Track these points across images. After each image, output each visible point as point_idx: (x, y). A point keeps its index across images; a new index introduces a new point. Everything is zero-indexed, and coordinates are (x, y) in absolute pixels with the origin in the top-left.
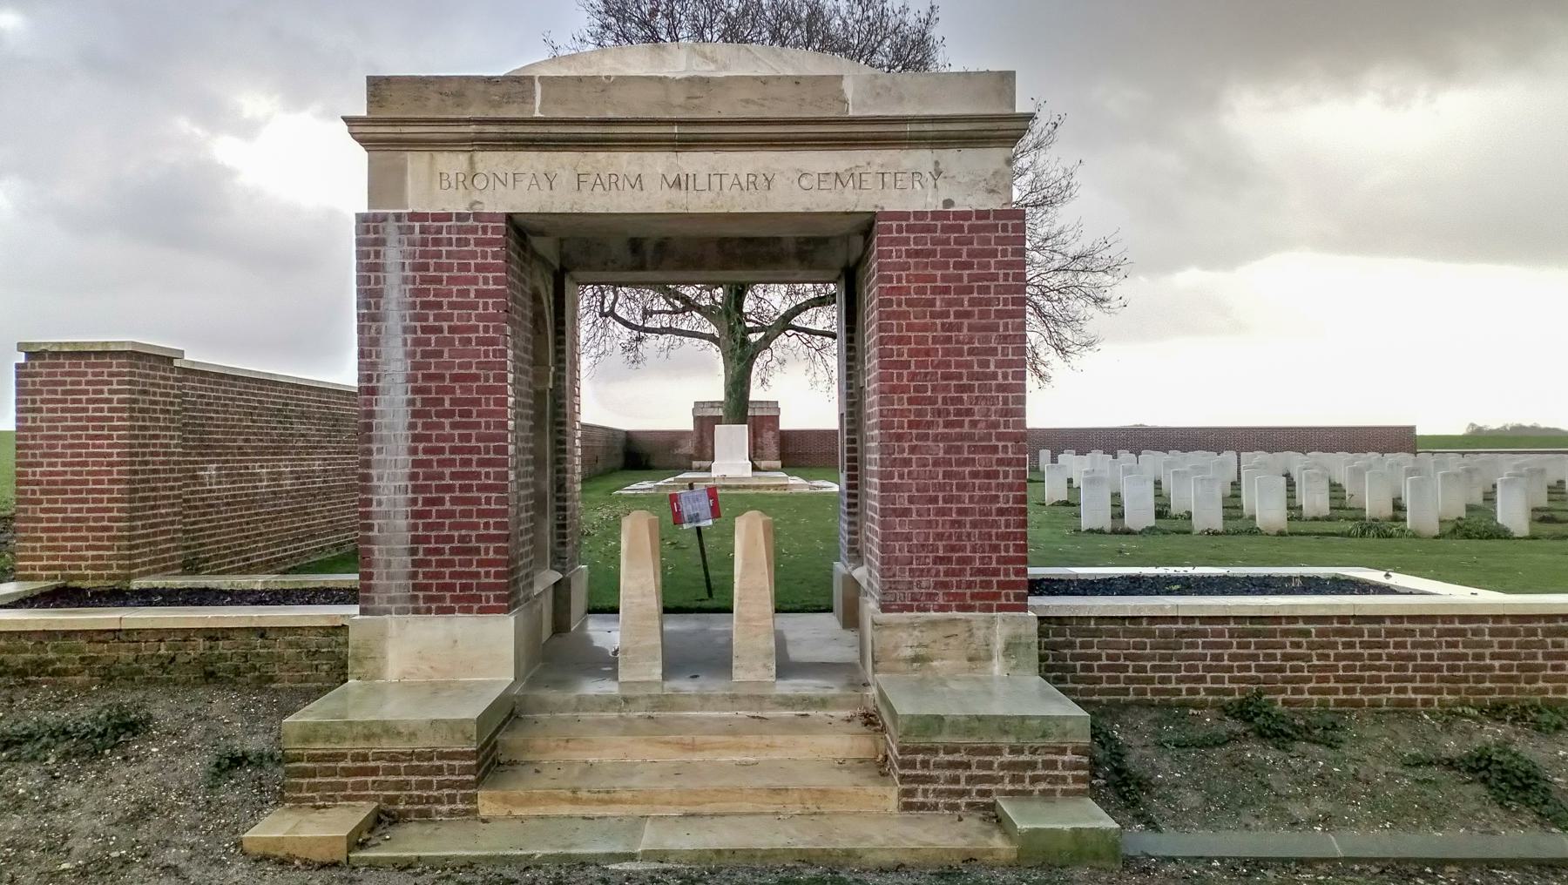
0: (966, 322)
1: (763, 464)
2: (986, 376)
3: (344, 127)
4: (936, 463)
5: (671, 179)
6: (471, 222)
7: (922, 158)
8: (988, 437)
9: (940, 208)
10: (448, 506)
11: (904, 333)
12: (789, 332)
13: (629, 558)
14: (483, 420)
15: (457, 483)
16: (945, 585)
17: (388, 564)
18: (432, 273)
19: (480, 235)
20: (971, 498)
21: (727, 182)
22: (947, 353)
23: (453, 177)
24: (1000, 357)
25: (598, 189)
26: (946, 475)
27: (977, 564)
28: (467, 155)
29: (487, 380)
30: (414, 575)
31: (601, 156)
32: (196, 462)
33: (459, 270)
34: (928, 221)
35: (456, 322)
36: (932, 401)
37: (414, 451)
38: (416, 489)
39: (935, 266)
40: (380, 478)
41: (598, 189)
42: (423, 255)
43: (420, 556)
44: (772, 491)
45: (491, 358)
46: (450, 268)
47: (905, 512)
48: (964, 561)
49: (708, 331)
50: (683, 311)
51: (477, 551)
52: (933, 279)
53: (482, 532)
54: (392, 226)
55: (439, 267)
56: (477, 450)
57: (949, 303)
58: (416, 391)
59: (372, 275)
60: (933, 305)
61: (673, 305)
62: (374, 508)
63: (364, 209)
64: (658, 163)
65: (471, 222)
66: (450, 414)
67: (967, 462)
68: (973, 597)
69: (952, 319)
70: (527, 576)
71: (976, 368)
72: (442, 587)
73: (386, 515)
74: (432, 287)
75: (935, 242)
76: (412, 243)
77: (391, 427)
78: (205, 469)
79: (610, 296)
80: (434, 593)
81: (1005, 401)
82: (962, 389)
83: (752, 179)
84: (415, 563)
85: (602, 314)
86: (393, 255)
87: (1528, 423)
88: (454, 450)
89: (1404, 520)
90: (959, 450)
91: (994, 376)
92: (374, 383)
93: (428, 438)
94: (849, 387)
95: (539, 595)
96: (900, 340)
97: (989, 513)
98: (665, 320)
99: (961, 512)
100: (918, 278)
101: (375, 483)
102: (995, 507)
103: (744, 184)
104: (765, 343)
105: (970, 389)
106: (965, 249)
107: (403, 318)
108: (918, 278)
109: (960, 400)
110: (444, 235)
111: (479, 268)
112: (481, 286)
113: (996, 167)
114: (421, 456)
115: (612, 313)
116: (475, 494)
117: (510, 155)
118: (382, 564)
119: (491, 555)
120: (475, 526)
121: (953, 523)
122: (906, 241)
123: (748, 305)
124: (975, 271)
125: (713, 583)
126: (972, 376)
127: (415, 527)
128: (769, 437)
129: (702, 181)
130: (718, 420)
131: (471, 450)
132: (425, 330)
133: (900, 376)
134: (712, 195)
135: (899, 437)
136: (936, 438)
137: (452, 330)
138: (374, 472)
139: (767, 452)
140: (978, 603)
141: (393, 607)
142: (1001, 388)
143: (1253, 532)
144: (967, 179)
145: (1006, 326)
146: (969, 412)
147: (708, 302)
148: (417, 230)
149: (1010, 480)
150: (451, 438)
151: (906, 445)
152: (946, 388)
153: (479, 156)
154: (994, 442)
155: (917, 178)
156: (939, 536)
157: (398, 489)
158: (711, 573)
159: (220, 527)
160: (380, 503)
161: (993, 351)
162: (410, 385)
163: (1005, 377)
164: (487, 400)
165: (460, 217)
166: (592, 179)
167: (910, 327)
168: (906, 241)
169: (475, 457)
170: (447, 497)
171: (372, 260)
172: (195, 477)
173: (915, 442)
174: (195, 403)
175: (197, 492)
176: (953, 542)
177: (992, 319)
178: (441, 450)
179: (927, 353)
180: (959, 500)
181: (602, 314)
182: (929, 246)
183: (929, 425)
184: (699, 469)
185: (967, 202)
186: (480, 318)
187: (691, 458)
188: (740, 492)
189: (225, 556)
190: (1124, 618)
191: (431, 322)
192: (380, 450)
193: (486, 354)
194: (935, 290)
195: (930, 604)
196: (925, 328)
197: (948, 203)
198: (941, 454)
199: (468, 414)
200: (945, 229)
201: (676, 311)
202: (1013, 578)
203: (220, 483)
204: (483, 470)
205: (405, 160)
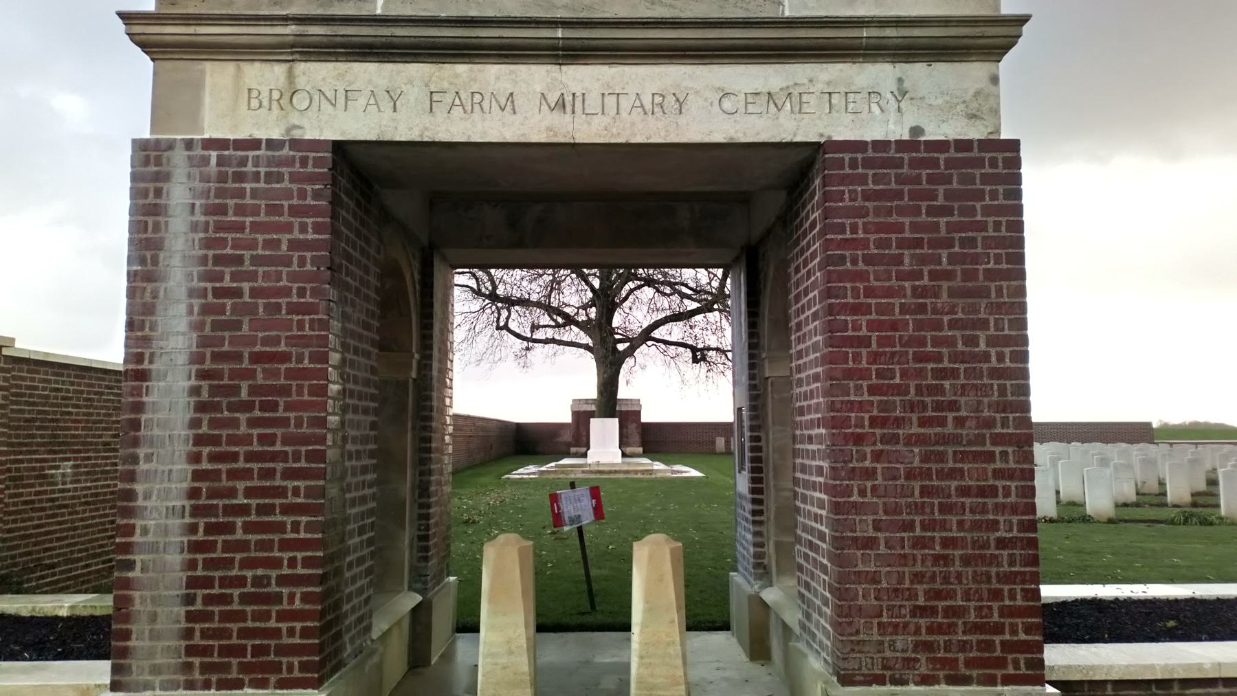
0: (945, 285)
1: (628, 450)
2: (975, 357)
3: (120, 25)
4: (910, 475)
5: (553, 98)
6: (286, 151)
7: (882, 74)
8: (980, 439)
9: (906, 137)
10: (239, 535)
11: (862, 300)
12: (649, 343)
13: (491, 601)
14: (292, 415)
15: (254, 502)
16: (928, 647)
17: (153, 618)
18: (231, 218)
19: (297, 168)
20: (960, 524)
21: (626, 103)
22: (919, 325)
23: (265, 94)
24: (992, 331)
25: (457, 111)
26: (925, 491)
27: (972, 617)
28: (284, 67)
29: (300, 360)
30: (188, 634)
31: (462, 69)
32: (45, 460)
33: (268, 213)
34: (892, 153)
35: (260, 283)
36: (901, 390)
37: (195, 458)
38: (197, 511)
39: (902, 211)
40: (147, 496)
41: (457, 111)
42: (220, 193)
43: (199, 606)
44: (639, 476)
45: (307, 332)
46: (255, 211)
47: (870, 543)
48: (952, 612)
49: (584, 342)
50: (564, 325)
51: (278, 598)
52: (899, 228)
53: (286, 571)
54: (179, 157)
55: (241, 210)
56: (283, 456)
57: (923, 260)
58: (202, 375)
59: (150, 220)
60: (901, 263)
61: (555, 321)
62: (137, 538)
63: (146, 135)
64: (535, 78)
65: (286, 151)
66: (247, 406)
67: (952, 474)
68: (969, 663)
69: (926, 281)
70: (360, 620)
71: (960, 347)
72: (228, 651)
73: (153, 548)
74: (230, 236)
75: (901, 180)
76: (205, 179)
77: (163, 424)
78: (57, 468)
79: (504, 313)
80: (216, 659)
81: (1002, 390)
82: (941, 374)
83: (658, 99)
84: (191, 617)
85: (498, 328)
86: (179, 194)
87: (1201, 419)
88: (252, 457)
89: (1218, 506)
90: (941, 457)
91: (986, 357)
92: (146, 365)
93: (215, 441)
94: (752, 377)
95: (385, 635)
96: (856, 309)
97: (985, 545)
98: (550, 333)
99: (947, 543)
100: (881, 228)
101: (140, 502)
102: (993, 536)
103: (648, 107)
104: (630, 352)
105: (954, 373)
106: (941, 189)
107: (189, 276)
108: (881, 228)
109: (939, 390)
110: (250, 168)
111: (294, 211)
112: (296, 235)
113: (978, 86)
114: (205, 465)
115: (506, 327)
116: (279, 518)
117: (342, 66)
118: (144, 617)
119: (297, 604)
120: (277, 563)
121: (936, 558)
122: (863, 180)
123: (617, 321)
124: (956, 218)
125: (595, 586)
126: (955, 357)
127: (192, 565)
128: (632, 427)
129: (593, 103)
130: (592, 414)
131: (274, 457)
132: (218, 293)
133: (857, 357)
134: (606, 120)
135: (859, 439)
136: (910, 441)
137: (255, 293)
138: (139, 488)
139: (631, 440)
140: (975, 673)
141: (158, 680)
142: (996, 373)
143: (1086, 519)
144: (940, 101)
145: (999, 291)
146: (953, 406)
147: (584, 318)
148: (213, 161)
149: (1013, 499)
150: (247, 440)
151: (868, 450)
152: (920, 373)
153: (301, 67)
154: (989, 447)
155: (874, 98)
156: (918, 577)
157: (171, 511)
158: (594, 572)
159: (75, 529)
160: (145, 531)
161: (984, 324)
162: (194, 368)
163: (1000, 358)
164: (300, 387)
165: (271, 144)
166: (448, 98)
167: (870, 292)
168: (863, 180)
169: (280, 466)
170: (239, 521)
171: (151, 199)
172: (45, 476)
173: (879, 447)
174: (47, 397)
175: (45, 492)
176: (937, 586)
177: (981, 281)
178: (234, 457)
179: (894, 326)
180: (943, 526)
181: (498, 328)
182: (893, 186)
183: (899, 422)
184: (576, 455)
185: (942, 129)
186: (293, 277)
187: (569, 445)
188: (612, 476)
189: (80, 559)
190: (1149, 682)
191: (227, 283)
192: (149, 458)
193: (301, 326)
194: (902, 244)
195: (909, 674)
196: (890, 292)
197: (917, 130)
198: (916, 463)
199: (274, 407)
200: (914, 164)
201: (558, 326)
202: (1023, 636)
203: (78, 481)
204: (291, 484)
205: (203, 72)
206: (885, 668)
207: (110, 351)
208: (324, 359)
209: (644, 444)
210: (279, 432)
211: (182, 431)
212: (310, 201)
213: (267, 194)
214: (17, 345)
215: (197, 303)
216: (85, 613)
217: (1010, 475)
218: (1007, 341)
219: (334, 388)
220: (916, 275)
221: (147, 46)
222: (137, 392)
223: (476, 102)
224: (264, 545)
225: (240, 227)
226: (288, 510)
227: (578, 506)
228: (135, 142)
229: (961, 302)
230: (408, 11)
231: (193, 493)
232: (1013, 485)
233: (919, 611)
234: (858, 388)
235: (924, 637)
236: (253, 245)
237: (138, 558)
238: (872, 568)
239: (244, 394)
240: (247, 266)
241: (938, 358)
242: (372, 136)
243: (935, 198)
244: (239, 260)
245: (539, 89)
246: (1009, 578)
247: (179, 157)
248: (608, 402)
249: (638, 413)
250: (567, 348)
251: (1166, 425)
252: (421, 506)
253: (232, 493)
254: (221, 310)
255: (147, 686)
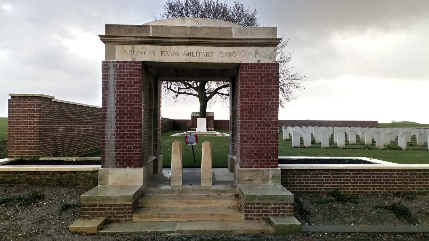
0: (263, 92)
1: (210, 129)
3: (99, 38)
4: (255, 129)
5: (186, 53)
7: (252, 49)
10: (125, 139)
12: (217, 94)
13: (174, 153)
16: (257, 161)
17: (109, 154)
18: (122, 77)
19: (135, 67)
20: (264, 138)
21: (201, 54)
22: (258, 100)
23: (128, 52)
25: (167, 56)
26: (258, 132)
27: (265, 155)
28: (132, 46)
30: (116, 157)
31: (168, 47)
34: (254, 66)
35: (128, 90)
36: (254, 113)
38: (117, 134)
39: (255, 77)
40: (107, 131)
41: (167, 56)
42: (120, 72)
43: (118, 152)
46: (127, 76)
47: (247, 142)
50: (189, 88)
51: (133, 151)
52: (254, 81)
54: (111, 65)
56: (133, 124)
57: (259, 87)
59: (106, 77)
61: (186, 86)
62: (106, 139)
64: (183, 49)
65: (133, 64)
66: (126, 114)
68: (264, 164)
69: (259, 91)
70: (147, 158)
71: (266, 104)
73: (109, 141)
74: (122, 81)
77: (110, 118)
79: (170, 84)
81: (273, 113)
83: (208, 54)
84: (117, 154)
85: (168, 89)
87: (406, 120)
88: (127, 124)
91: (270, 106)
92: (106, 106)
93: (120, 121)
94: (232, 109)
95: (150, 163)
96: (246, 97)
97: (268, 142)
98: (184, 91)
99: (261, 142)
100: (251, 81)
101: (106, 132)
102: (270, 140)
103: (206, 55)
104: (210, 97)
105: (264, 110)
106: (263, 73)
107: (114, 89)
108: (251, 81)
109: (261, 113)
110: (126, 67)
111: (135, 76)
112: (135, 81)
114: (118, 126)
115: (170, 88)
117: (143, 46)
118: (108, 154)
119: (137, 152)
120: (133, 144)
121: (259, 145)
122: (248, 71)
123: (206, 87)
126: (265, 106)
127: (117, 144)
128: (211, 121)
129: (194, 54)
130: (198, 117)
131: (132, 124)
132: (120, 92)
133: (246, 106)
134: (197, 58)
135: (245, 122)
138: (106, 130)
140: (265, 166)
141: (111, 166)
142: (272, 110)
146: (264, 116)
148: (118, 65)
149: (274, 134)
150: (127, 121)
151: (247, 124)
152: (258, 109)
153: (135, 46)
154: (270, 124)
156: (256, 148)
157: (112, 134)
158: (196, 157)
160: (107, 138)
161: (270, 100)
163: (273, 107)
164: (137, 111)
165: (130, 62)
166: (165, 53)
167: (249, 93)
168: (248, 71)
169: (133, 126)
170: (125, 136)
171: (106, 73)
172: (57, 131)
174: (57, 111)
178: (124, 124)
179: (253, 100)
180: (261, 139)
181: (168, 89)
182: (254, 72)
183: (253, 119)
184: (193, 130)
186: (135, 89)
187: (191, 127)
189: (65, 152)
191: (122, 90)
192: (107, 124)
193: (136, 99)
194: (255, 84)
196: (252, 94)
197: (259, 61)
198: (256, 127)
200: (258, 68)
201: (187, 88)
202: (275, 159)
203: (64, 132)
204: (135, 129)
206: (248, 165)
207: (98, 103)
208: (141, 105)
209: (214, 127)
210: (133, 119)
211: (113, 119)
212: (138, 74)
213: (129, 72)
214: (55, 98)
215: (116, 94)
216: (79, 160)
217: (274, 129)
218: (274, 103)
219: (143, 111)
220: (258, 90)
221: (104, 41)
222: (105, 111)
223: (171, 54)
224: (130, 141)
225: (124, 79)
226: (135, 134)
227: (192, 139)
228: (102, 61)
229: (266, 96)
230: (157, 36)
231: (116, 131)
232: (274, 131)
233: (255, 154)
234: (246, 112)
235: (256, 159)
236: (126, 83)
237: (106, 143)
238: (247, 146)
239: (126, 112)
240: (126, 87)
241: (261, 106)
242: (150, 61)
243: (262, 75)
244: (124, 86)
245: (183, 51)
246: (273, 148)
247: (111, 65)
248: (203, 113)
249: (213, 117)
250: (190, 96)
251: (394, 122)
252: (155, 137)
253: (124, 131)
254: (121, 95)
255: (109, 167)
